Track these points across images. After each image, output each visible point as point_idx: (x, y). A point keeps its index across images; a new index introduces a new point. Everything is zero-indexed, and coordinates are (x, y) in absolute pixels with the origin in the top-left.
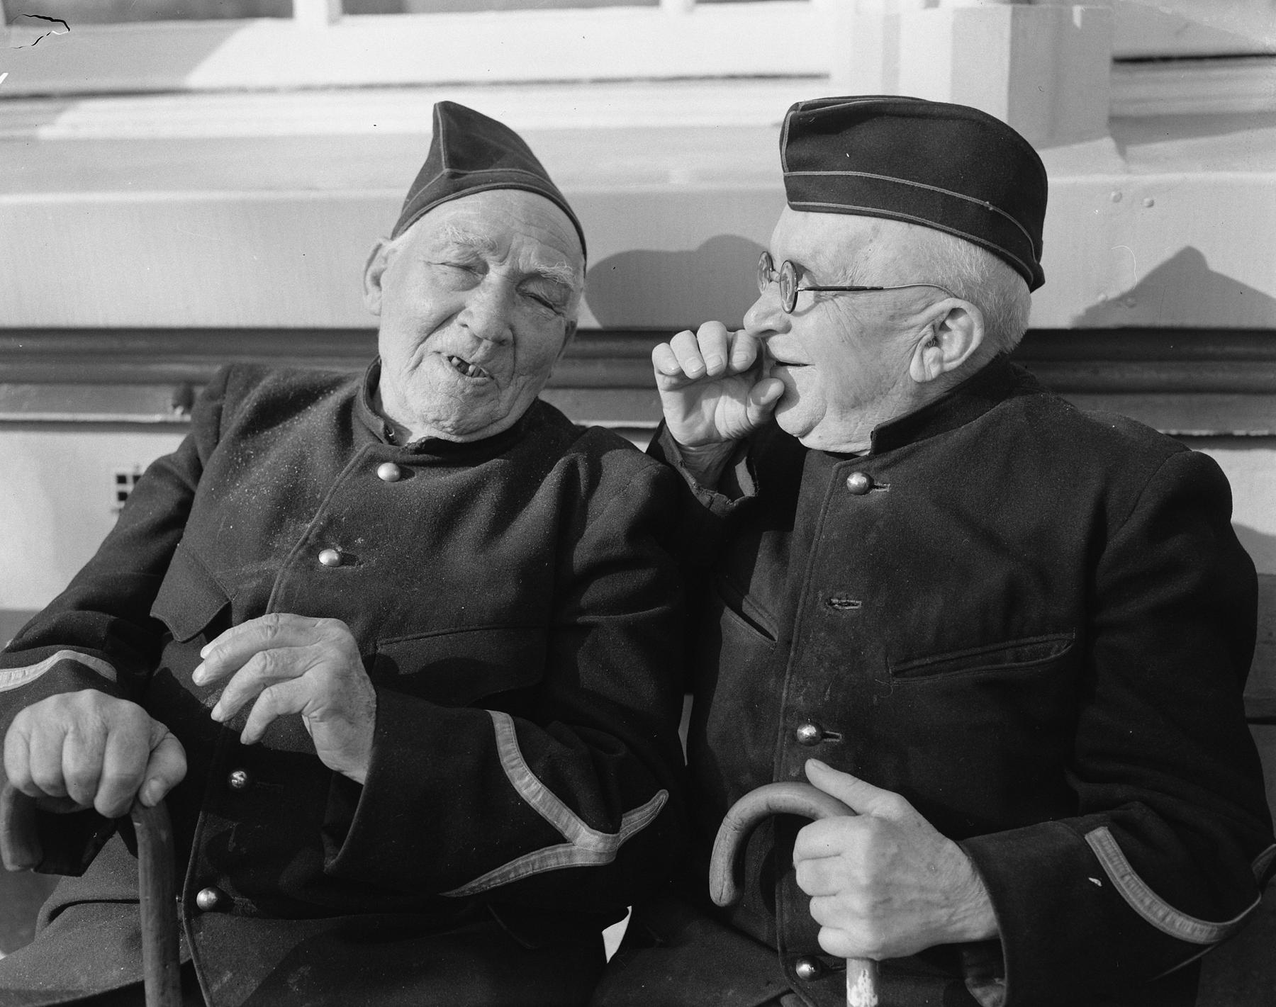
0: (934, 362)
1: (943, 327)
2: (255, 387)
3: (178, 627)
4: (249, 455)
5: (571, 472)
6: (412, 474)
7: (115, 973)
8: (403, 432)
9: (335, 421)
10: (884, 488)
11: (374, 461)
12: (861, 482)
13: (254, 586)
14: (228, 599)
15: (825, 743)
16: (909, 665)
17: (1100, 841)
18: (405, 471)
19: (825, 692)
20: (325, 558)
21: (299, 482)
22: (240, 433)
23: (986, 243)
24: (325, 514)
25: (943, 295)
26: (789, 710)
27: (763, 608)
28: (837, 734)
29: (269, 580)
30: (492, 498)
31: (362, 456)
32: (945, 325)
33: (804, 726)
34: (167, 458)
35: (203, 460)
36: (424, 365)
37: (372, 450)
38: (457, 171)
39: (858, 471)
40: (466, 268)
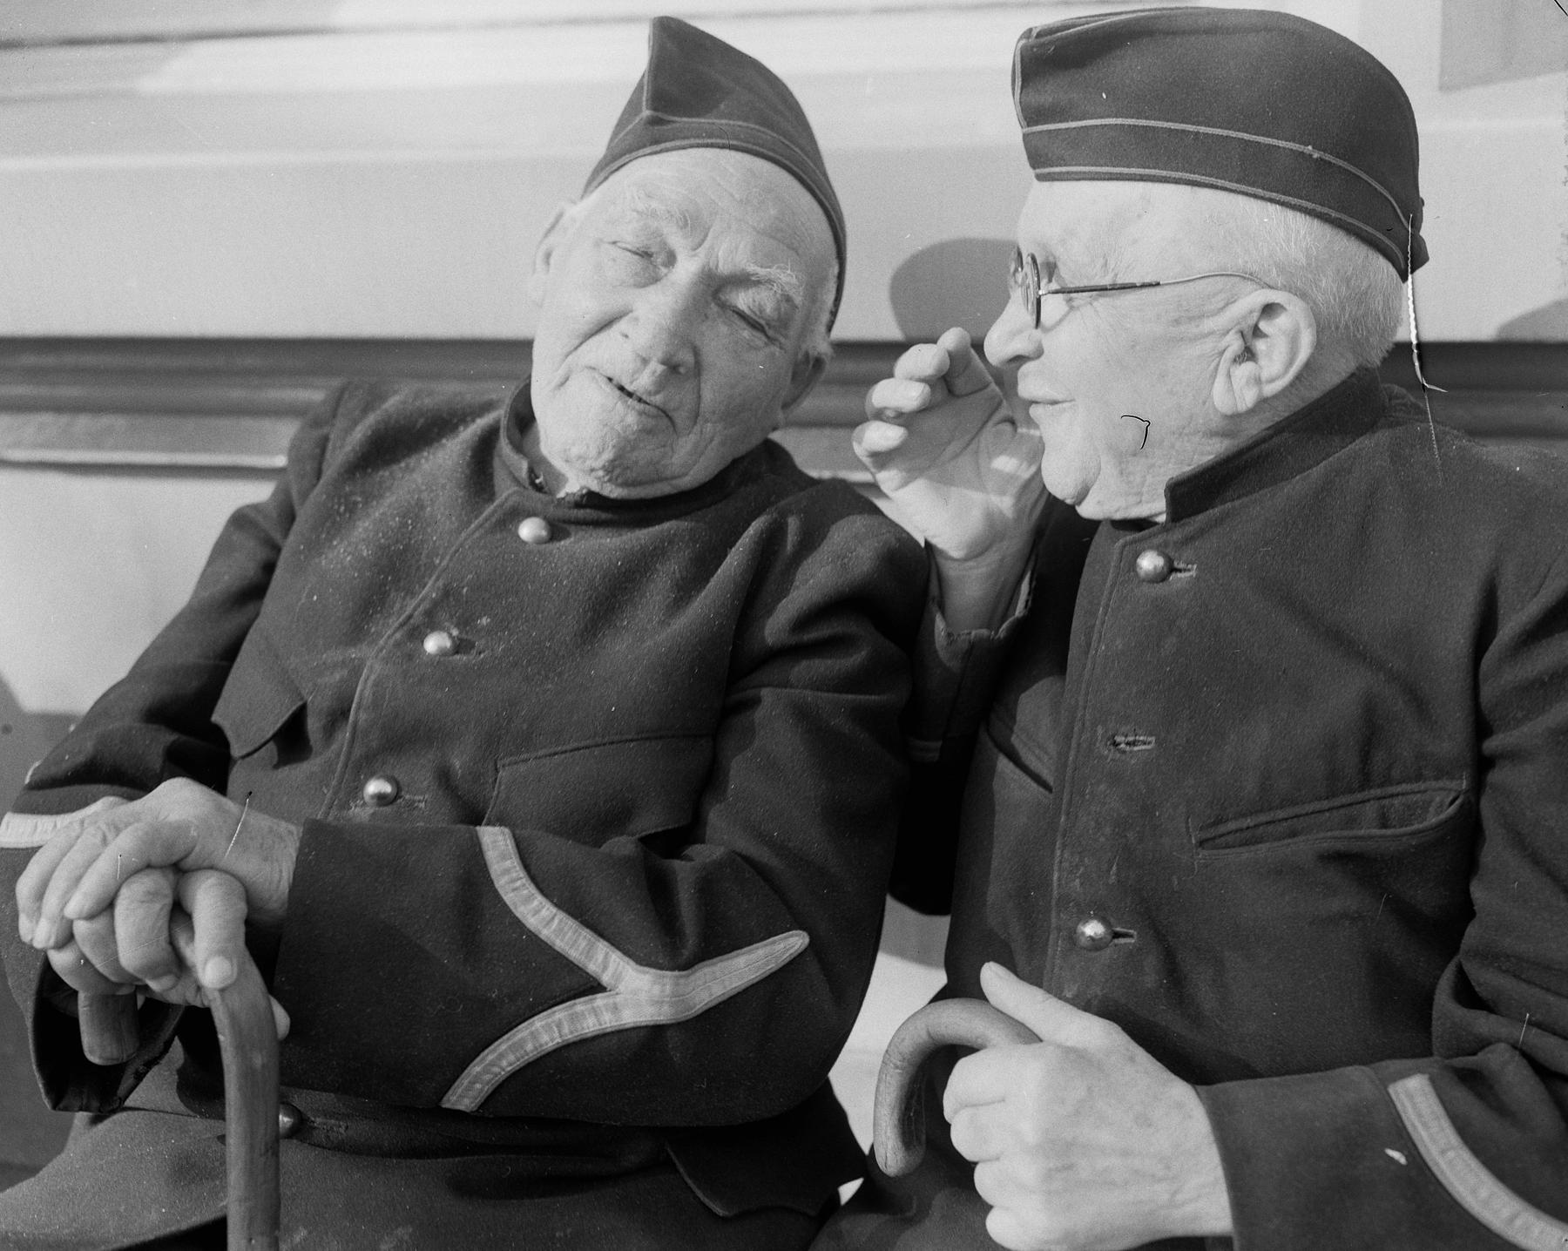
0: (1248, 383)
1: (1257, 332)
2: (466, 426)
3: (239, 736)
4: (355, 503)
5: (770, 542)
6: (567, 535)
7: (154, 1216)
8: (559, 478)
9: (468, 458)
10: (1189, 570)
11: (516, 514)
12: (1157, 563)
13: (337, 680)
14: (302, 699)
15: (1116, 945)
16: (1222, 829)
17: (1411, 1097)
18: (556, 530)
19: (1108, 871)
20: (433, 643)
21: (413, 542)
22: (346, 471)
23: (1310, 205)
24: (440, 583)
25: (1250, 286)
26: (1064, 901)
27: (1040, 747)
28: (1131, 931)
29: (356, 672)
30: (674, 573)
31: (501, 506)
32: (1259, 329)
33: (1086, 922)
34: (255, 507)
35: (296, 508)
36: (572, 385)
37: (515, 498)
38: (660, 115)
39: (1151, 548)
40: (645, 255)
